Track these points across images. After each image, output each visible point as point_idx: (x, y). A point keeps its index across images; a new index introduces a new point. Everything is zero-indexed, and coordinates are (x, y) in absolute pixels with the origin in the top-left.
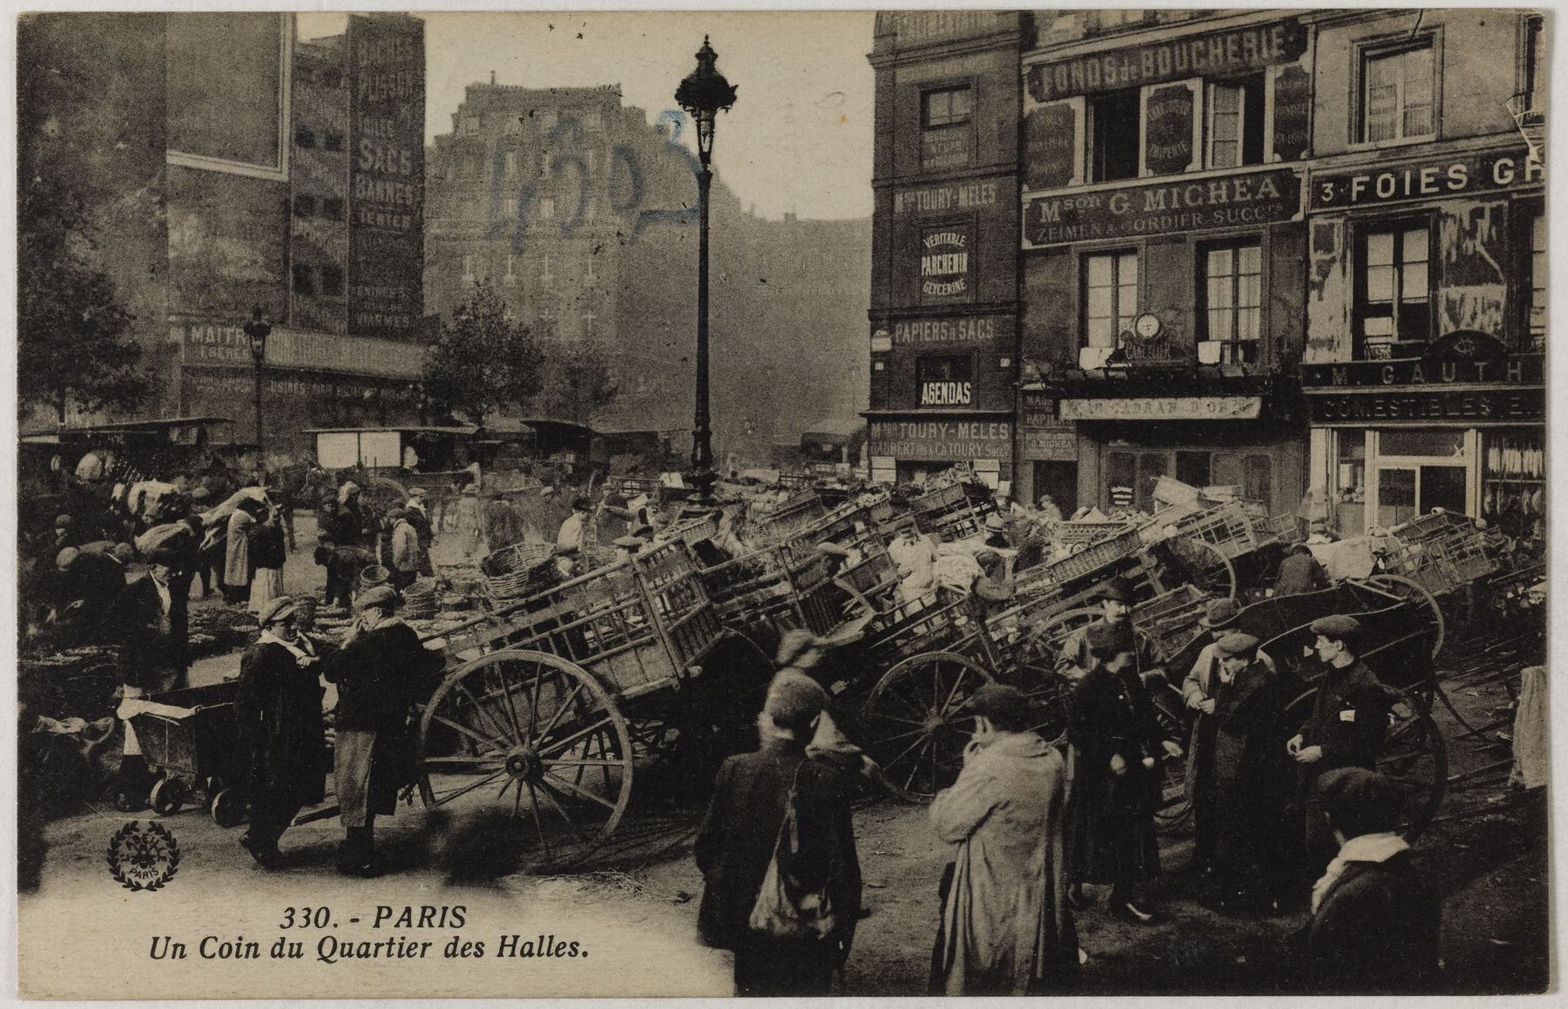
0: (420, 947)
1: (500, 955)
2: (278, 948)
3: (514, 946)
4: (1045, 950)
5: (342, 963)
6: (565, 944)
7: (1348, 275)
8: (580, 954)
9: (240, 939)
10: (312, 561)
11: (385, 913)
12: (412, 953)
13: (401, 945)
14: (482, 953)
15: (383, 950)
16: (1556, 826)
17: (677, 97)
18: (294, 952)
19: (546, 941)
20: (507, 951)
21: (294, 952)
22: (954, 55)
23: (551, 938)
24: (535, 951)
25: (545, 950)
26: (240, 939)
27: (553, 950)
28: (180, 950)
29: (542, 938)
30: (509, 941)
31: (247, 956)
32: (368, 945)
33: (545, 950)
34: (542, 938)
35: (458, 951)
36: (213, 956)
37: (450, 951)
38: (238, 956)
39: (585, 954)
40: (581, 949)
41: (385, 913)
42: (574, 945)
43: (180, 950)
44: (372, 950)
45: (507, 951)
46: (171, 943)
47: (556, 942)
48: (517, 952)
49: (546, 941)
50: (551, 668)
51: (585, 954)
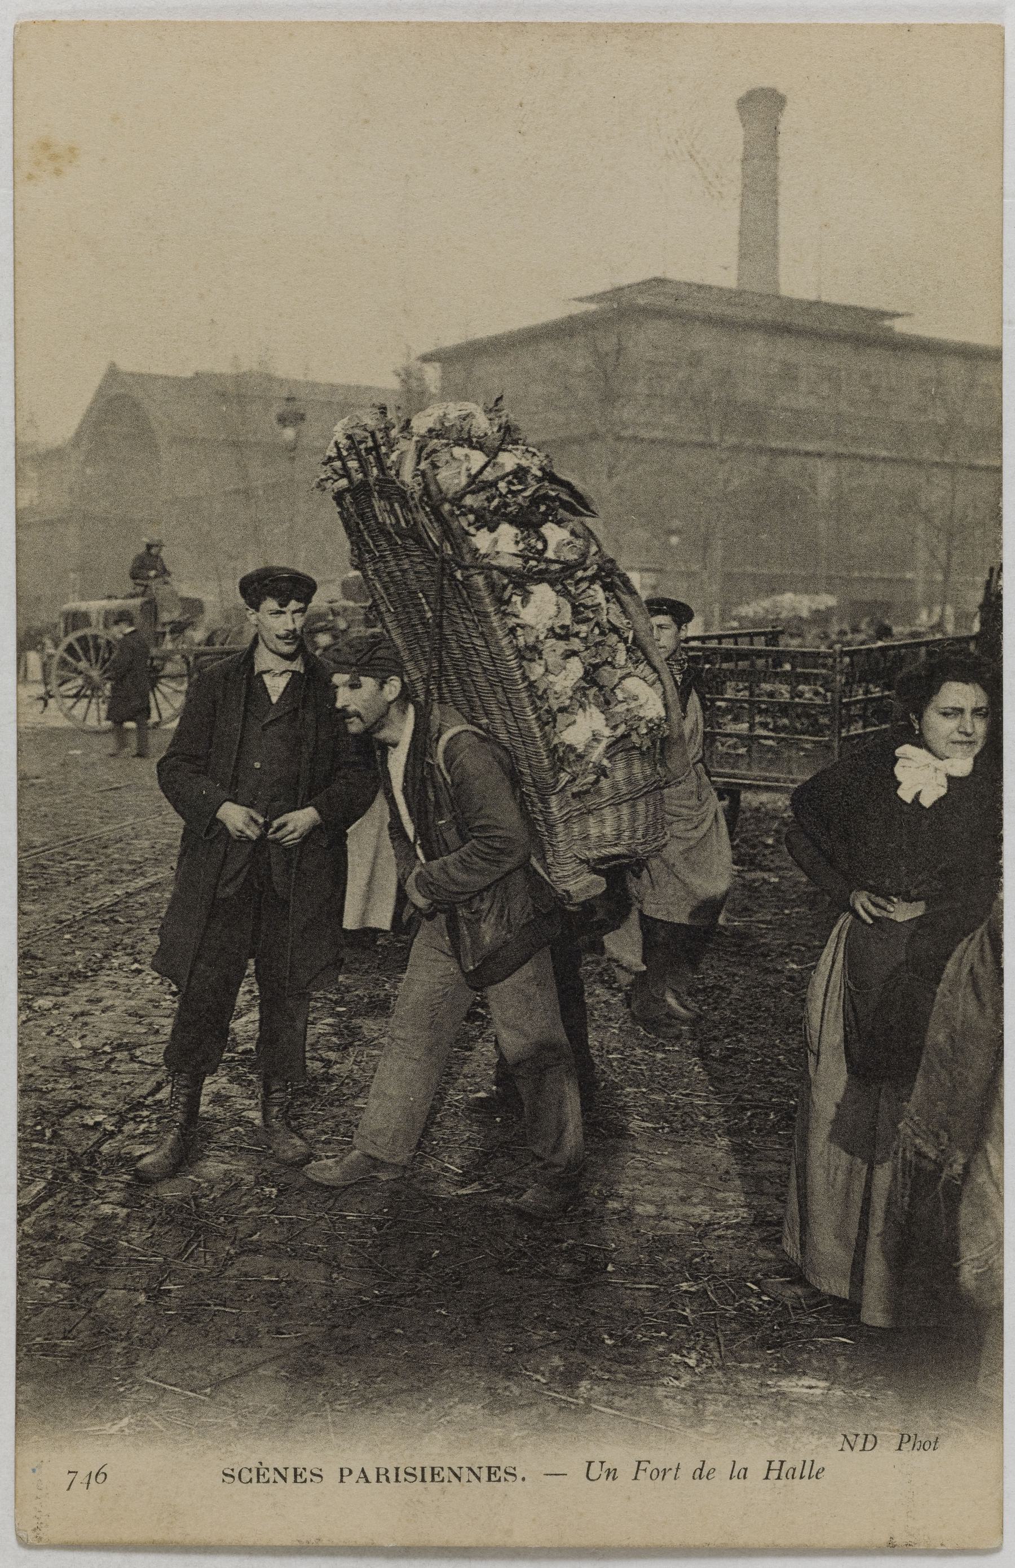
19: (808, 1464)
24: (797, 1474)
28: (612, 1474)
30: (776, 1465)
43: (612, 1474)
46: (606, 1466)
48: (783, 1475)
49: (808, 1464)
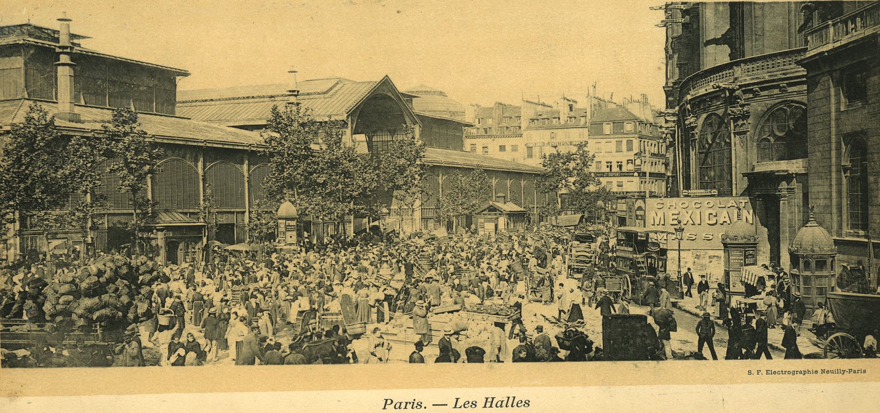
3: (492, 402)
4: (198, 189)
7: (521, 394)
8: (423, 407)
9: (414, 400)
11: (389, 402)
15: (409, 406)
16: (300, 396)
19: (511, 400)
20: (488, 404)
23: (514, 397)
24: (504, 404)
26: (414, 400)
27: (515, 404)
36: (461, 407)
39: (572, 291)
41: (389, 402)
44: (403, 405)
45: (488, 404)
48: (494, 405)
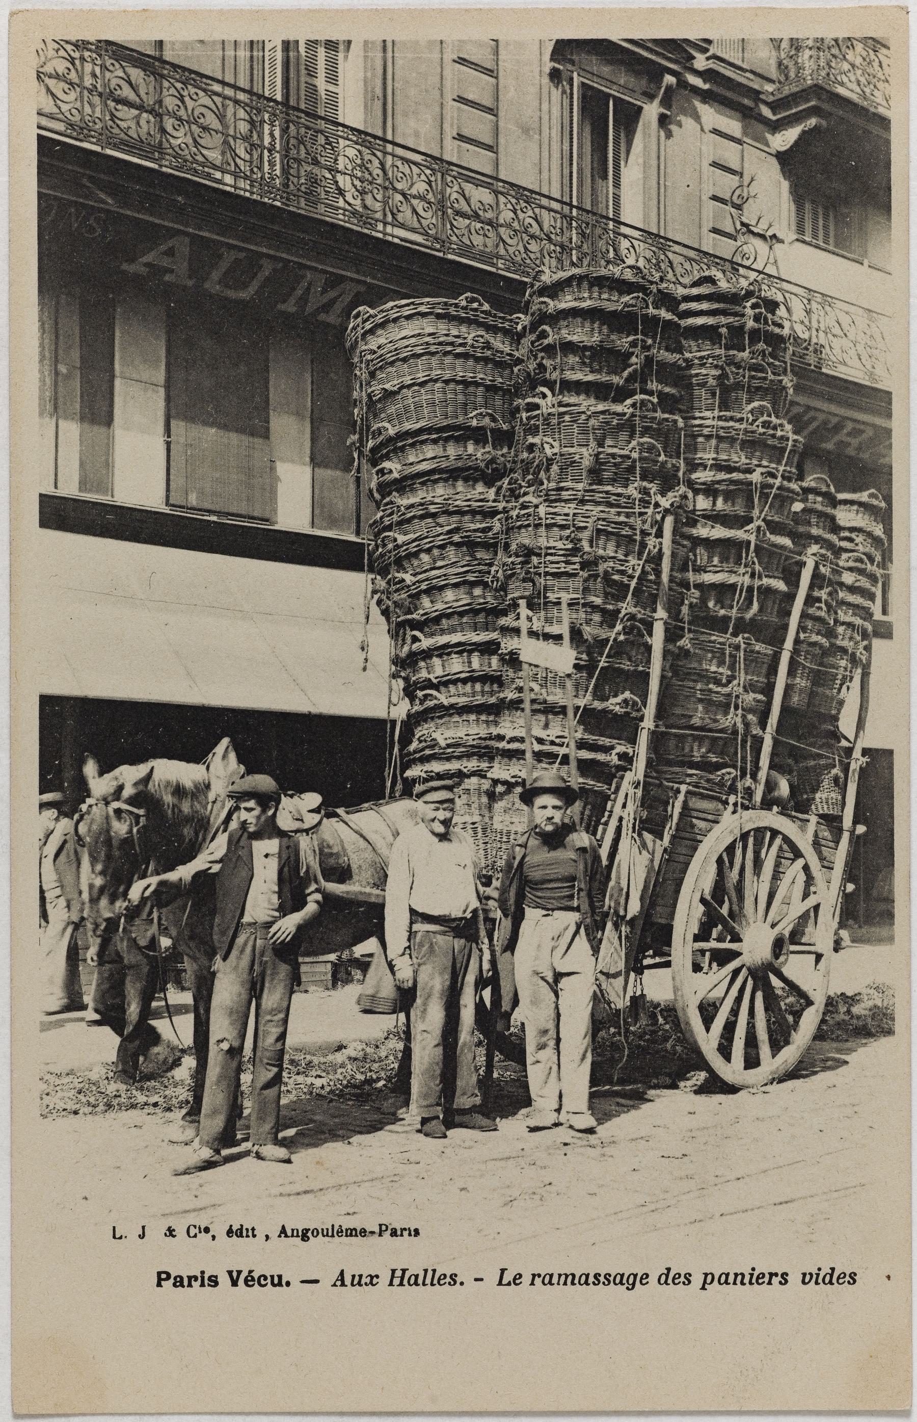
0: (767, 1276)
1: (391, 1284)
2: (663, 1278)
3: (402, 1278)
5: (349, 1291)
6: (445, 1276)
10: (355, 999)
12: (841, 1281)
13: (752, 1275)
14: (690, 1282)
17: (889, 394)
18: (356, 1282)
20: (397, 1281)
21: (356, 1282)
22: (726, 98)
23: (434, 1271)
25: (428, 1281)
29: (426, 1271)
30: (399, 1273)
31: (735, 1283)
32: (727, 1275)
33: (428, 1281)
34: (426, 1271)
35: (834, 1280)
37: (662, 1281)
38: (817, 1283)
39: (462, 1284)
40: (458, 1280)
42: (453, 1277)
43: (214, 1281)
45: (397, 1281)
47: (756, 1274)
48: (405, 1282)
50: (796, 1022)
51: (462, 1284)
